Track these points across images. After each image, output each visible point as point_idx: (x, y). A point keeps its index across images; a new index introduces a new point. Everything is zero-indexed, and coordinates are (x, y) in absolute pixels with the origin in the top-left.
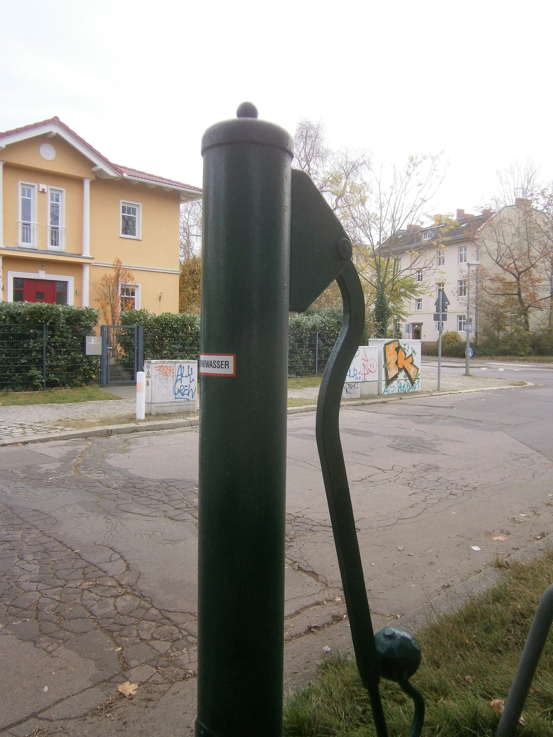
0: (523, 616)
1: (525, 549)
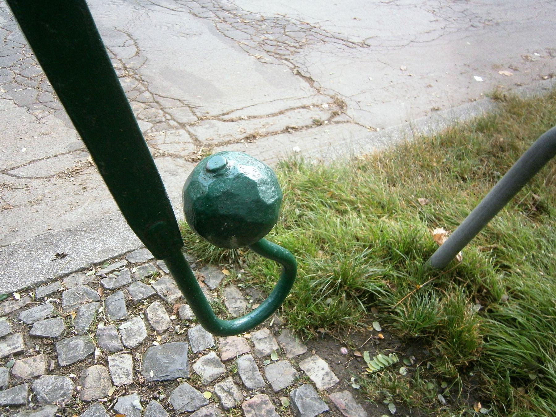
0: (502, 149)
1: (527, 86)
